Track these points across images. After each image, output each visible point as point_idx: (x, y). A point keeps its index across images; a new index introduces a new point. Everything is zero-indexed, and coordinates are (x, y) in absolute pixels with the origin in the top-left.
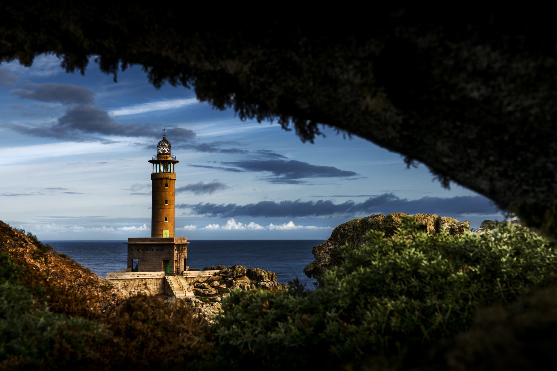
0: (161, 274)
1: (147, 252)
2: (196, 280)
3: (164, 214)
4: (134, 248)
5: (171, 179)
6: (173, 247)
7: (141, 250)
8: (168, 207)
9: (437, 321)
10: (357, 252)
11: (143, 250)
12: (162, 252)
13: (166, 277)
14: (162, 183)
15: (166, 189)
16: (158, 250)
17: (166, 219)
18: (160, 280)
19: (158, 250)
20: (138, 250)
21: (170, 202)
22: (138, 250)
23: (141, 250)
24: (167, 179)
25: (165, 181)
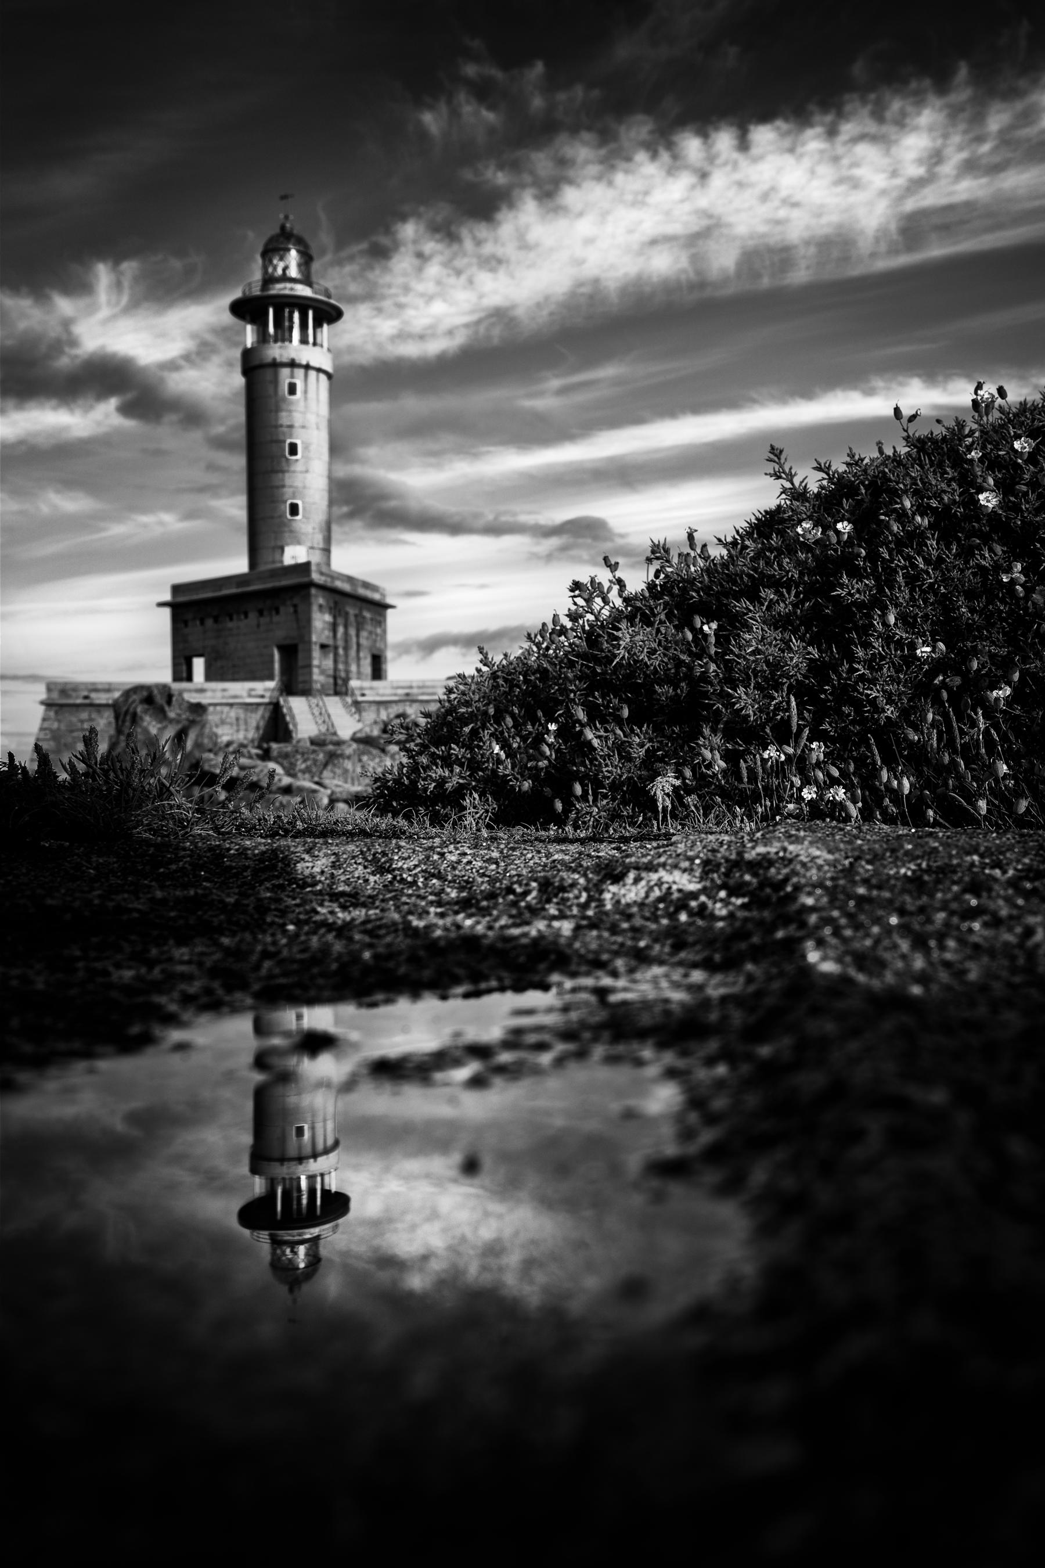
0: (265, 688)
1: (230, 625)
2: (394, 710)
3: (288, 491)
4: (189, 616)
5: (307, 367)
6: (307, 599)
7: (209, 622)
8: (299, 467)
9: (100, 752)
10: (551, 740)
11: (216, 620)
12: (276, 618)
13: (281, 701)
14: (276, 382)
15: (291, 403)
16: (261, 613)
17: (294, 509)
18: (261, 711)
19: (261, 613)
20: (202, 623)
21: (306, 448)
22: (202, 623)
23: (209, 622)
24: (293, 364)
25: (285, 372)
